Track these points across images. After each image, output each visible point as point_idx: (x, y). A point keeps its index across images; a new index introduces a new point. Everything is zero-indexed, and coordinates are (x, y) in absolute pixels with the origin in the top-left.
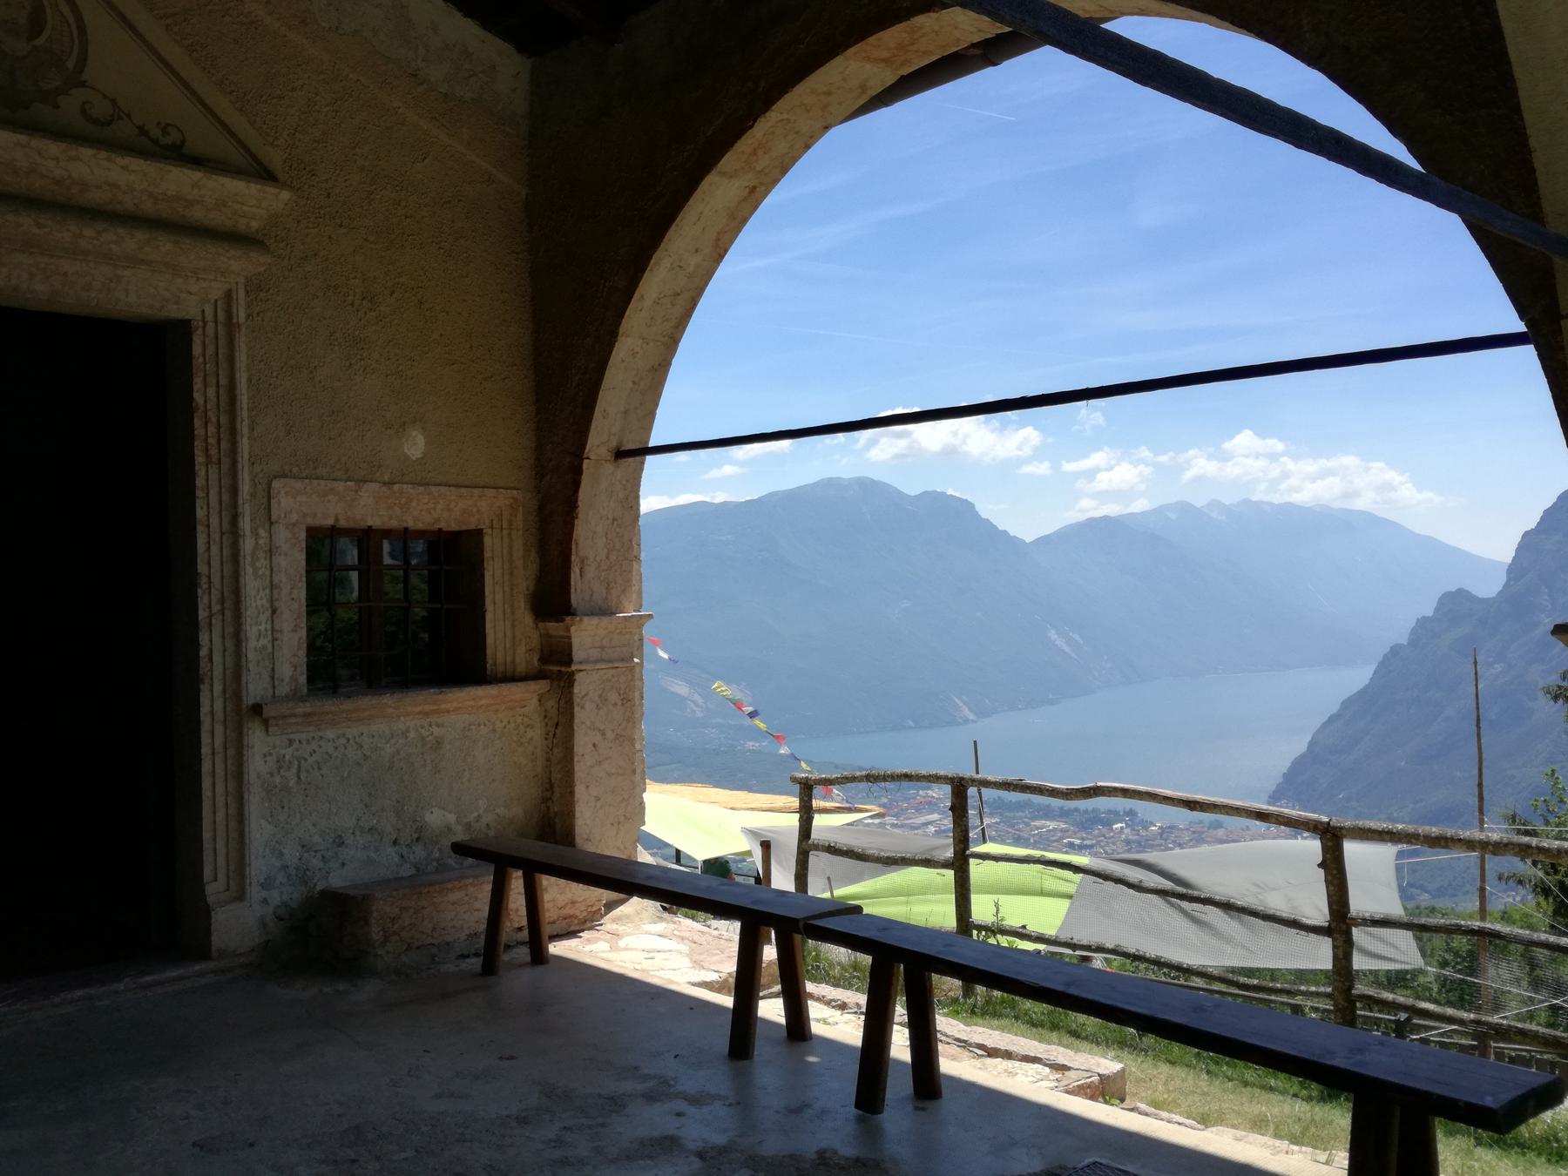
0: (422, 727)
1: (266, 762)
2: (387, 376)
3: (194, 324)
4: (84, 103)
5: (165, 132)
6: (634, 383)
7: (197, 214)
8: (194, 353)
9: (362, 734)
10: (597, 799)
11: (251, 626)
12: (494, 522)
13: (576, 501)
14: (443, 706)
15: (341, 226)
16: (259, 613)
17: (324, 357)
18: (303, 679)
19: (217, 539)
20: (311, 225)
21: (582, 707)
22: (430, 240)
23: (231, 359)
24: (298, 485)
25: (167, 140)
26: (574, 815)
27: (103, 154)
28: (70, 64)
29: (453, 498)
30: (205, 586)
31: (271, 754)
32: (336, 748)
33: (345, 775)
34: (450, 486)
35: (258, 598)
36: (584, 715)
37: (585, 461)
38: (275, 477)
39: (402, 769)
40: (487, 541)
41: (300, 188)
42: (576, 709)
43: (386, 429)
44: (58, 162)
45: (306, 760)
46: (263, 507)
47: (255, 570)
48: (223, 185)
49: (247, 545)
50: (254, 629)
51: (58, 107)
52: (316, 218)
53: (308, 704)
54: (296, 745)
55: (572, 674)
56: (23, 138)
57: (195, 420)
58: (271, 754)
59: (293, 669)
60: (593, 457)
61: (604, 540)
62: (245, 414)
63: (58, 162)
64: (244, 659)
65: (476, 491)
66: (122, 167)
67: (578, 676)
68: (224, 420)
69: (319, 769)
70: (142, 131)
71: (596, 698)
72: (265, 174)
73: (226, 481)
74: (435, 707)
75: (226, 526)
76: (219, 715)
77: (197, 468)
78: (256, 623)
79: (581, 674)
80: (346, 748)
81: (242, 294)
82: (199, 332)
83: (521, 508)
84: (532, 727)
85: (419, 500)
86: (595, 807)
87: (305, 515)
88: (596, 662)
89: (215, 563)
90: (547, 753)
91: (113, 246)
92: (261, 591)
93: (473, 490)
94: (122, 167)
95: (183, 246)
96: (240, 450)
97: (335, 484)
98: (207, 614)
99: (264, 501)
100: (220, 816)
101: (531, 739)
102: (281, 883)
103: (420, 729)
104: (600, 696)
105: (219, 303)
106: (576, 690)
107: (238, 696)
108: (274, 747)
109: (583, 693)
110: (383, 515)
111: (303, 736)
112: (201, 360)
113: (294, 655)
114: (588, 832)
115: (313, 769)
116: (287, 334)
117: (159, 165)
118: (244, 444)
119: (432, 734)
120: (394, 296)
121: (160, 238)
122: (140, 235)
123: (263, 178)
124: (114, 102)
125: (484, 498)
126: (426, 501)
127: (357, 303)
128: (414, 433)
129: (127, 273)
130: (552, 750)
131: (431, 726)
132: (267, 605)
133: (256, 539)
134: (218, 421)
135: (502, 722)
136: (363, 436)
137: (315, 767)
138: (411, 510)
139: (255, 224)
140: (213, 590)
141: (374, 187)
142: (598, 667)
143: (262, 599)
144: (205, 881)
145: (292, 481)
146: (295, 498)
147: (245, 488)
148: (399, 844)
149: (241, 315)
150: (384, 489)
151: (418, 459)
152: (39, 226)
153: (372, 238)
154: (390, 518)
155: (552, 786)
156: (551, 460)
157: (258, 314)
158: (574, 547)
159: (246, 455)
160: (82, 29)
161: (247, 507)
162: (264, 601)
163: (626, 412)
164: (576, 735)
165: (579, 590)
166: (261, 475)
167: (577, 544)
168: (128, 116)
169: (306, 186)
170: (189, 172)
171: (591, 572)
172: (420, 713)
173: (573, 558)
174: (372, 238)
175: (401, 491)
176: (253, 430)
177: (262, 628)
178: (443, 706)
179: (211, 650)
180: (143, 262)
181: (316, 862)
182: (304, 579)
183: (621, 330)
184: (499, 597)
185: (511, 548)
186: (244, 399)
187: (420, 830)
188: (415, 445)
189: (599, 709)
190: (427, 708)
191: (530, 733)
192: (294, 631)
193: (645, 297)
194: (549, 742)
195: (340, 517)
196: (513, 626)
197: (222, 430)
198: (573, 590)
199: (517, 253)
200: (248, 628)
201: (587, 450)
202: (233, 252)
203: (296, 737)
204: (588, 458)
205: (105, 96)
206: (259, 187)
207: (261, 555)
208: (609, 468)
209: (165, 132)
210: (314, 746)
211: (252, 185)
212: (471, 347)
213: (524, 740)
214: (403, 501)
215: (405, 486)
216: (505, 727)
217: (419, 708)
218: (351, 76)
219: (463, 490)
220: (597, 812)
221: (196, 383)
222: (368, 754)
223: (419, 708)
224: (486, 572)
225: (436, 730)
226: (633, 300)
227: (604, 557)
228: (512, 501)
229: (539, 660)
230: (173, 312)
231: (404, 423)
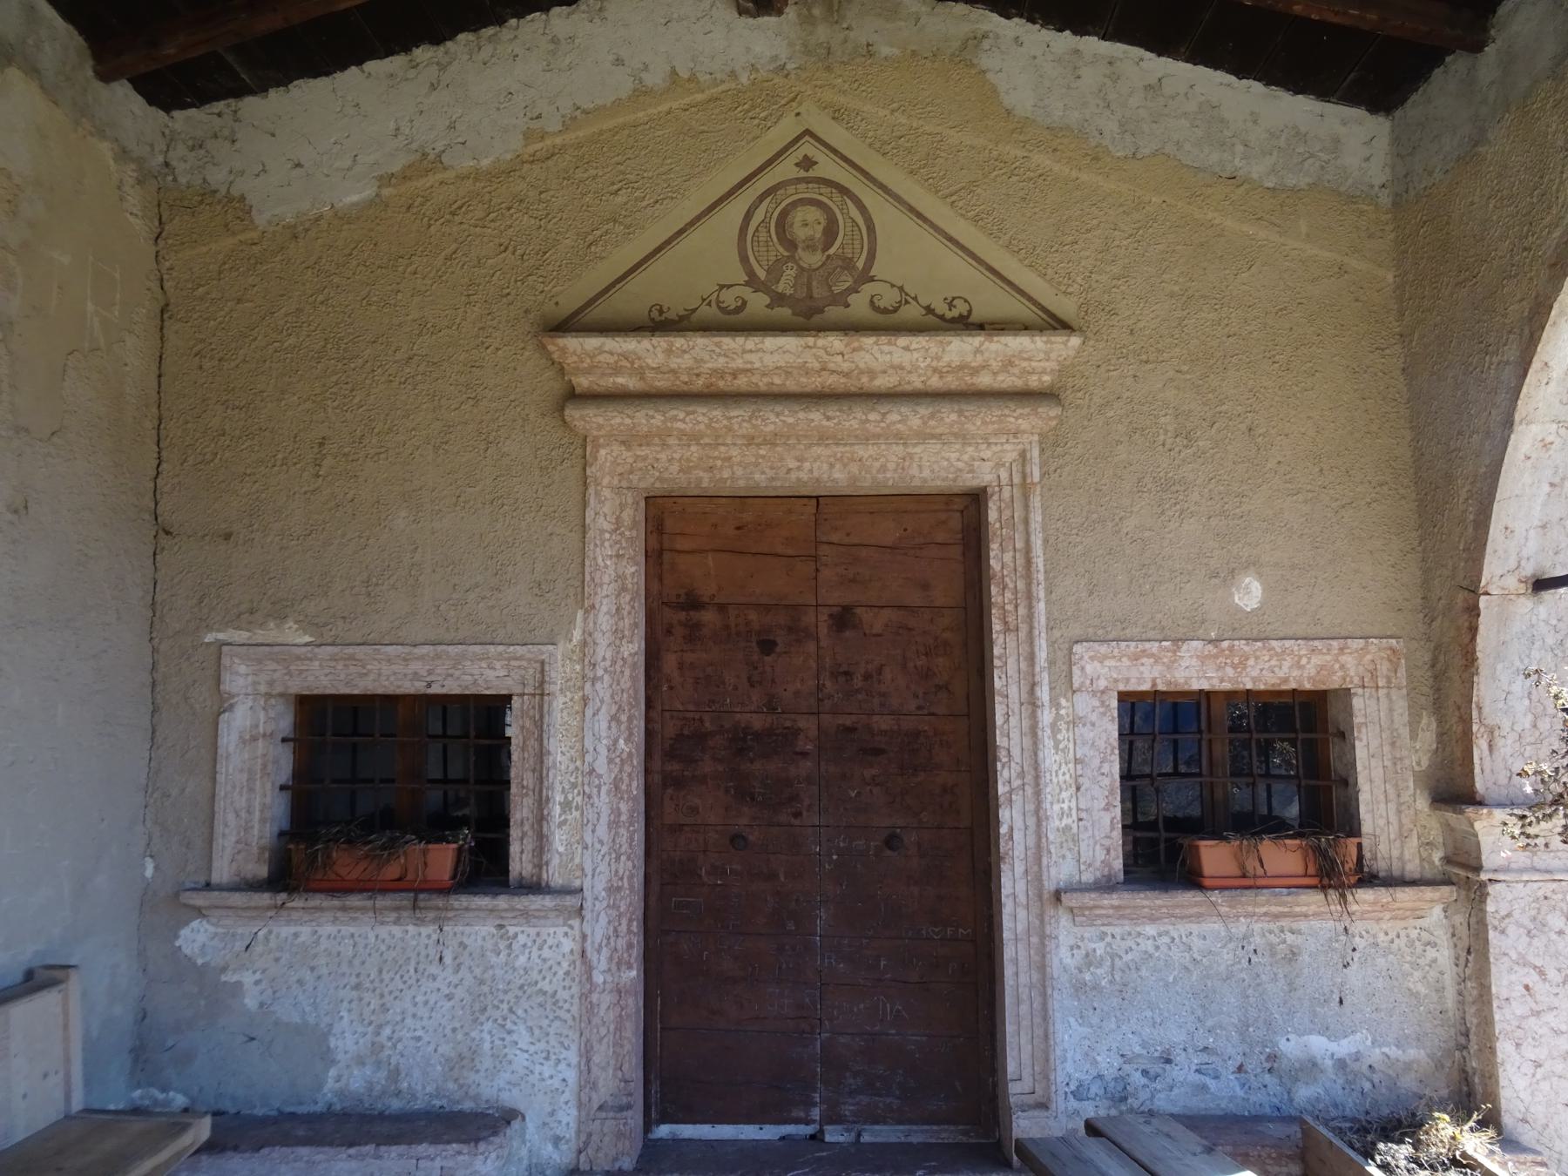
0: (1271, 932)
1: (1073, 955)
2: (1210, 518)
3: (989, 490)
4: (872, 302)
5: (951, 306)
6: (1552, 485)
7: (984, 381)
8: (990, 519)
9: (1191, 933)
10: (1538, 1065)
11: (1052, 804)
12: (1366, 680)
13: (1474, 652)
14: (1297, 909)
15: (1146, 362)
16: (1061, 790)
17: (1131, 506)
18: (1118, 864)
19: (1017, 710)
20: (1112, 368)
21: (1503, 932)
22: (1261, 356)
23: (1026, 522)
24: (1104, 649)
25: (955, 313)
26: (1497, 1082)
27: (884, 339)
28: (860, 264)
29: (1303, 652)
30: (1005, 760)
31: (1079, 947)
32: (1157, 948)
33: (1171, 979)
34: (1297, 639)
35: (1060, 773)
36: (1504, 944)
37: (1483, 598)
38: (1077, 642)
39: (1244, 981)
40: (1357, 703)
41: (1098, 331)
42: (1492, 934)
43: (1210, 578)
44: (843, 356)
45: (1121, 957)
46: (1064, 674)
47: (1057, 743)
48: (1006, 345)
49: (1046, 717)
50: (1056, 807)
51: (848, 306)
52: (1119, 358)
53: (1114, 896)
54: (1109, 939)
55: (1483, 885)
56: (810, 341)
57: (992, 587)
58: (1079, 947)
59: (1105, 852)
60: (1493, 590)
61: (1527, 702)
62: (1041, 577)
63: (843, 356)
64: (1044, 840)
65: (1335, 643)
66: (903, 348)
67: (1491, 889)
68: (1021, 585)
69: (1138, 969)
70: (929, 310)
71: (1527, 922)
72: (1058, 324)
73: (1024, 649)
74: (1286, 910)
75: (1024, 696)
76: (1022, 898)
77: (994, 636)
78: (1058, 801)
79: (1498, 886)
80: (1170, 949)
81: (1036, 452)
82: (995, 497)
83: (1403, 661)
84: (1435, 945)
85: (1257, 658)
86: (1534, 1075)
87: (1116, 681)
88: (1522, 871)
89: (1015, 735)
90: (1459, 984)
91: (899, 426)
92: (1063, 765)
93: (1331, 642)
94: (903, 348)
95: (966, 414)
96: (1036, 615)
97: (1147, 645)
98: (1007, 788)
99: (1065, 667)
100: (1024, 1008)
101: (1435, 961)
102: (1096, 1095)
103: (1267, 934)
104: (1534, 919)
105: (1014, 465)
106: (1490, 907)
107: (1039, 878)
108: (1082, 938)
109: (1503, 913)
110: (1212, 677)
111: (1117, 931)
112: (997, 525)
113: (1108, 837)
114: (1523, 1110)
115: (1130, 969)
116: (1087, 488)
117: (938, 338)
118: (1041, 607)
119: (1284, 942)
120: (1215, 427)
121: (943, 410)
122: (924, 410)
123: (1055, 329)
124: (901, 289)
125: (1346, 651)
126: (1266, 658)
127: (1169, 441)
128: (1247, 580)
129: (918, 449)
130: (1464, 981)
131: (1282, 931)
132: (1072, 781)
133: (1057, 709)
134: (1016, 587)
135: (1387, 934)
136: (1181, 588)
137: (1133, 967)
138: (1248, 670)
139: (1047, 378)
140: (1012, 763)
141: (1187, 311)
142: (1525, 877)
143: (1064, 774)
144: (1009, 1077)
145: (1096, 645)
146: (1101, 662)
147: (1042, 655)
148: (1246, 1072)
149: (1036, 474)
150: (1210, 647)
151: (1253, 610)
152: (828, 418)
153: (1185, 368)
154: (1222, 681)
155: (1467, 1035)
156: (1440, 599)
157: (1055, 471)
158: (1475, 714)
159: (1043, 620)
160: (871, 228)
161: (1045, 675)
162: (1067, 776)
163: (1544, 527)
164: (1494, 969)
165: (1487, 771)
166: (1061, 641)
167: (1480, 709)
168: (915, 299)
169: (1105, 329)
170: (970, 339)
171: (1506, 746)
172: (1265, 914)
173: (1475, 728)
174: (1185, 368)
175: (1231, 648)
176: (1051, 592)
177: (1065, 806)
178: (1297, 909)
179: (1011, 829)
180: (933, 436)
181: (1137, 1078)
182: (1117, 752)
183: (1517, 417)
184: (1378, 773)
185: (1391, 710)
186: (1039, 562)
187: (1272, 1057)
188: (1250, 594)
189: (1532, 938)
190: (1275, 909)
191: (1431, 953)
192: (1106, 809)
193: (1550, 364)
194: (1460, 969)
195: (1158, 681)
196: (1399, 812)
197: (1019, 595)
198: (1477, 770)
199: (1383, 350)
200: (1048, 806)
201: (1482, 584)
202: (1019, 411)
203: (1109, 930)
204: (1487, 594)
205: (893, 286)
206: (1044, 339)
207: (1063, 726)
208: (1525, 605)
209: (951, 306)
210: (1130, 943)
211: (1037, 338)
212: (1321, 470)
213: (1421, 962)
214: (1236, 660)
215: (1236, 643)
216: (1392, 942)
217: (1264, 910)
218: (1154, 199)
219: (1316, 643)
220: (1537, 1083)
221: (993, 550)
222: (1199, 958)
223: (1264, 910)
224: (1357, 743)
225: (1290, 938)
226: (1531, 370)
227: (1528, 726)
228: (1389, 652)
229: (1441, 859)
230: (969, 481)
231: (1234, 569)
